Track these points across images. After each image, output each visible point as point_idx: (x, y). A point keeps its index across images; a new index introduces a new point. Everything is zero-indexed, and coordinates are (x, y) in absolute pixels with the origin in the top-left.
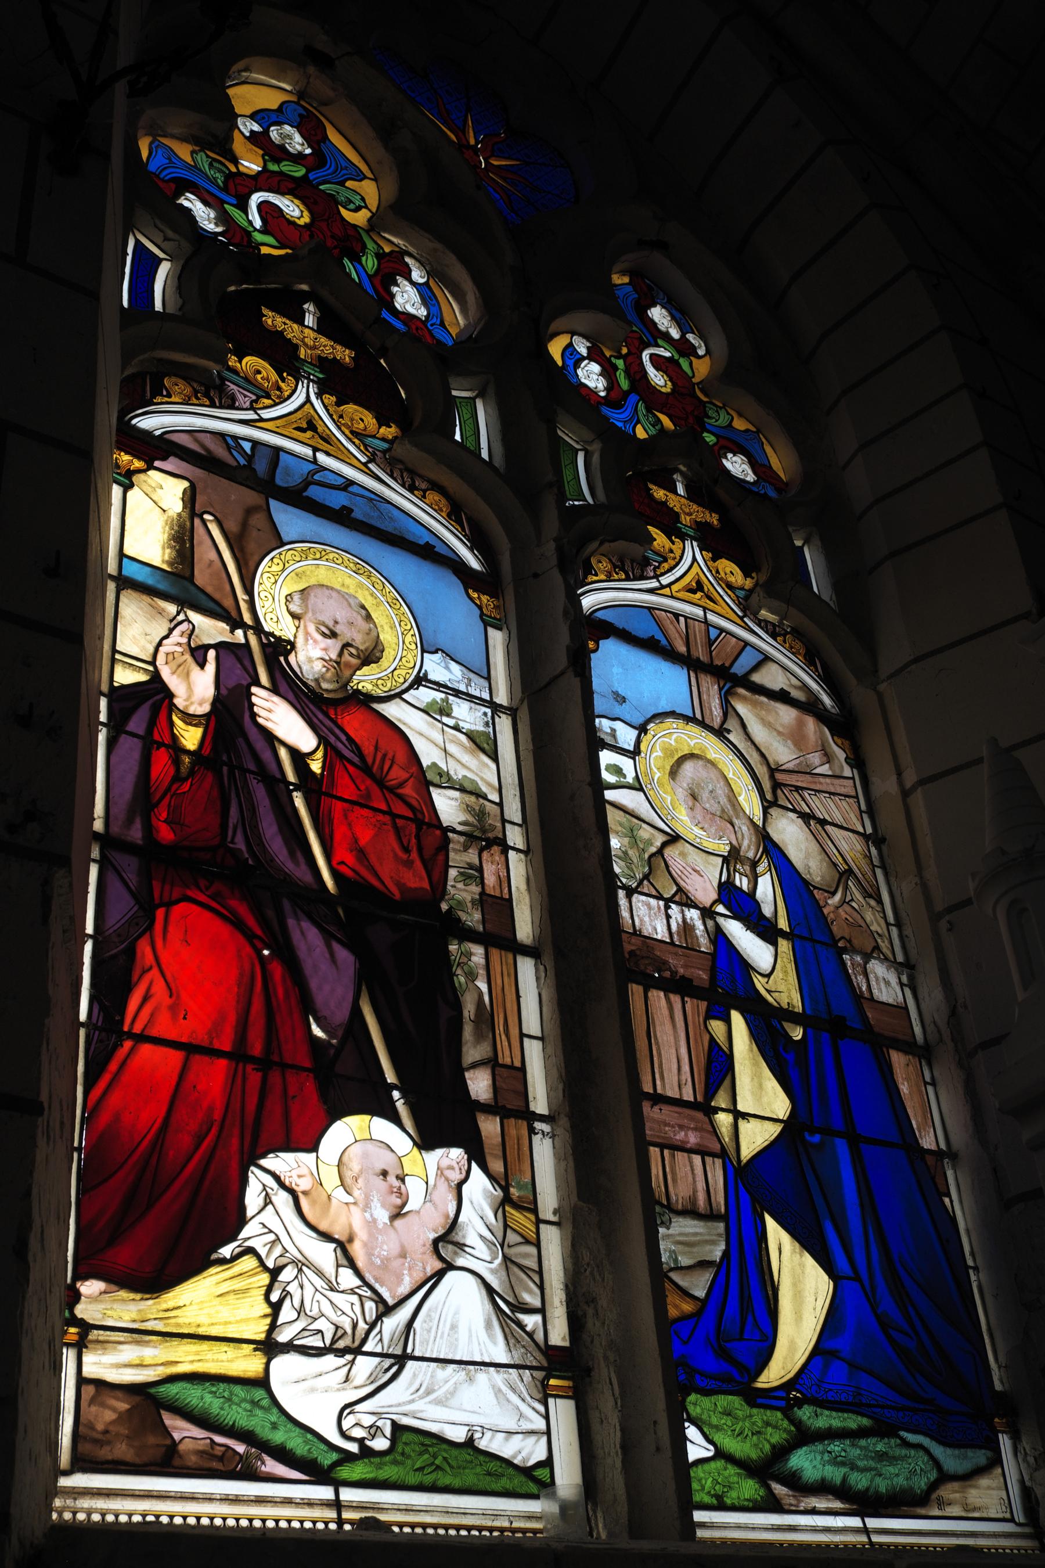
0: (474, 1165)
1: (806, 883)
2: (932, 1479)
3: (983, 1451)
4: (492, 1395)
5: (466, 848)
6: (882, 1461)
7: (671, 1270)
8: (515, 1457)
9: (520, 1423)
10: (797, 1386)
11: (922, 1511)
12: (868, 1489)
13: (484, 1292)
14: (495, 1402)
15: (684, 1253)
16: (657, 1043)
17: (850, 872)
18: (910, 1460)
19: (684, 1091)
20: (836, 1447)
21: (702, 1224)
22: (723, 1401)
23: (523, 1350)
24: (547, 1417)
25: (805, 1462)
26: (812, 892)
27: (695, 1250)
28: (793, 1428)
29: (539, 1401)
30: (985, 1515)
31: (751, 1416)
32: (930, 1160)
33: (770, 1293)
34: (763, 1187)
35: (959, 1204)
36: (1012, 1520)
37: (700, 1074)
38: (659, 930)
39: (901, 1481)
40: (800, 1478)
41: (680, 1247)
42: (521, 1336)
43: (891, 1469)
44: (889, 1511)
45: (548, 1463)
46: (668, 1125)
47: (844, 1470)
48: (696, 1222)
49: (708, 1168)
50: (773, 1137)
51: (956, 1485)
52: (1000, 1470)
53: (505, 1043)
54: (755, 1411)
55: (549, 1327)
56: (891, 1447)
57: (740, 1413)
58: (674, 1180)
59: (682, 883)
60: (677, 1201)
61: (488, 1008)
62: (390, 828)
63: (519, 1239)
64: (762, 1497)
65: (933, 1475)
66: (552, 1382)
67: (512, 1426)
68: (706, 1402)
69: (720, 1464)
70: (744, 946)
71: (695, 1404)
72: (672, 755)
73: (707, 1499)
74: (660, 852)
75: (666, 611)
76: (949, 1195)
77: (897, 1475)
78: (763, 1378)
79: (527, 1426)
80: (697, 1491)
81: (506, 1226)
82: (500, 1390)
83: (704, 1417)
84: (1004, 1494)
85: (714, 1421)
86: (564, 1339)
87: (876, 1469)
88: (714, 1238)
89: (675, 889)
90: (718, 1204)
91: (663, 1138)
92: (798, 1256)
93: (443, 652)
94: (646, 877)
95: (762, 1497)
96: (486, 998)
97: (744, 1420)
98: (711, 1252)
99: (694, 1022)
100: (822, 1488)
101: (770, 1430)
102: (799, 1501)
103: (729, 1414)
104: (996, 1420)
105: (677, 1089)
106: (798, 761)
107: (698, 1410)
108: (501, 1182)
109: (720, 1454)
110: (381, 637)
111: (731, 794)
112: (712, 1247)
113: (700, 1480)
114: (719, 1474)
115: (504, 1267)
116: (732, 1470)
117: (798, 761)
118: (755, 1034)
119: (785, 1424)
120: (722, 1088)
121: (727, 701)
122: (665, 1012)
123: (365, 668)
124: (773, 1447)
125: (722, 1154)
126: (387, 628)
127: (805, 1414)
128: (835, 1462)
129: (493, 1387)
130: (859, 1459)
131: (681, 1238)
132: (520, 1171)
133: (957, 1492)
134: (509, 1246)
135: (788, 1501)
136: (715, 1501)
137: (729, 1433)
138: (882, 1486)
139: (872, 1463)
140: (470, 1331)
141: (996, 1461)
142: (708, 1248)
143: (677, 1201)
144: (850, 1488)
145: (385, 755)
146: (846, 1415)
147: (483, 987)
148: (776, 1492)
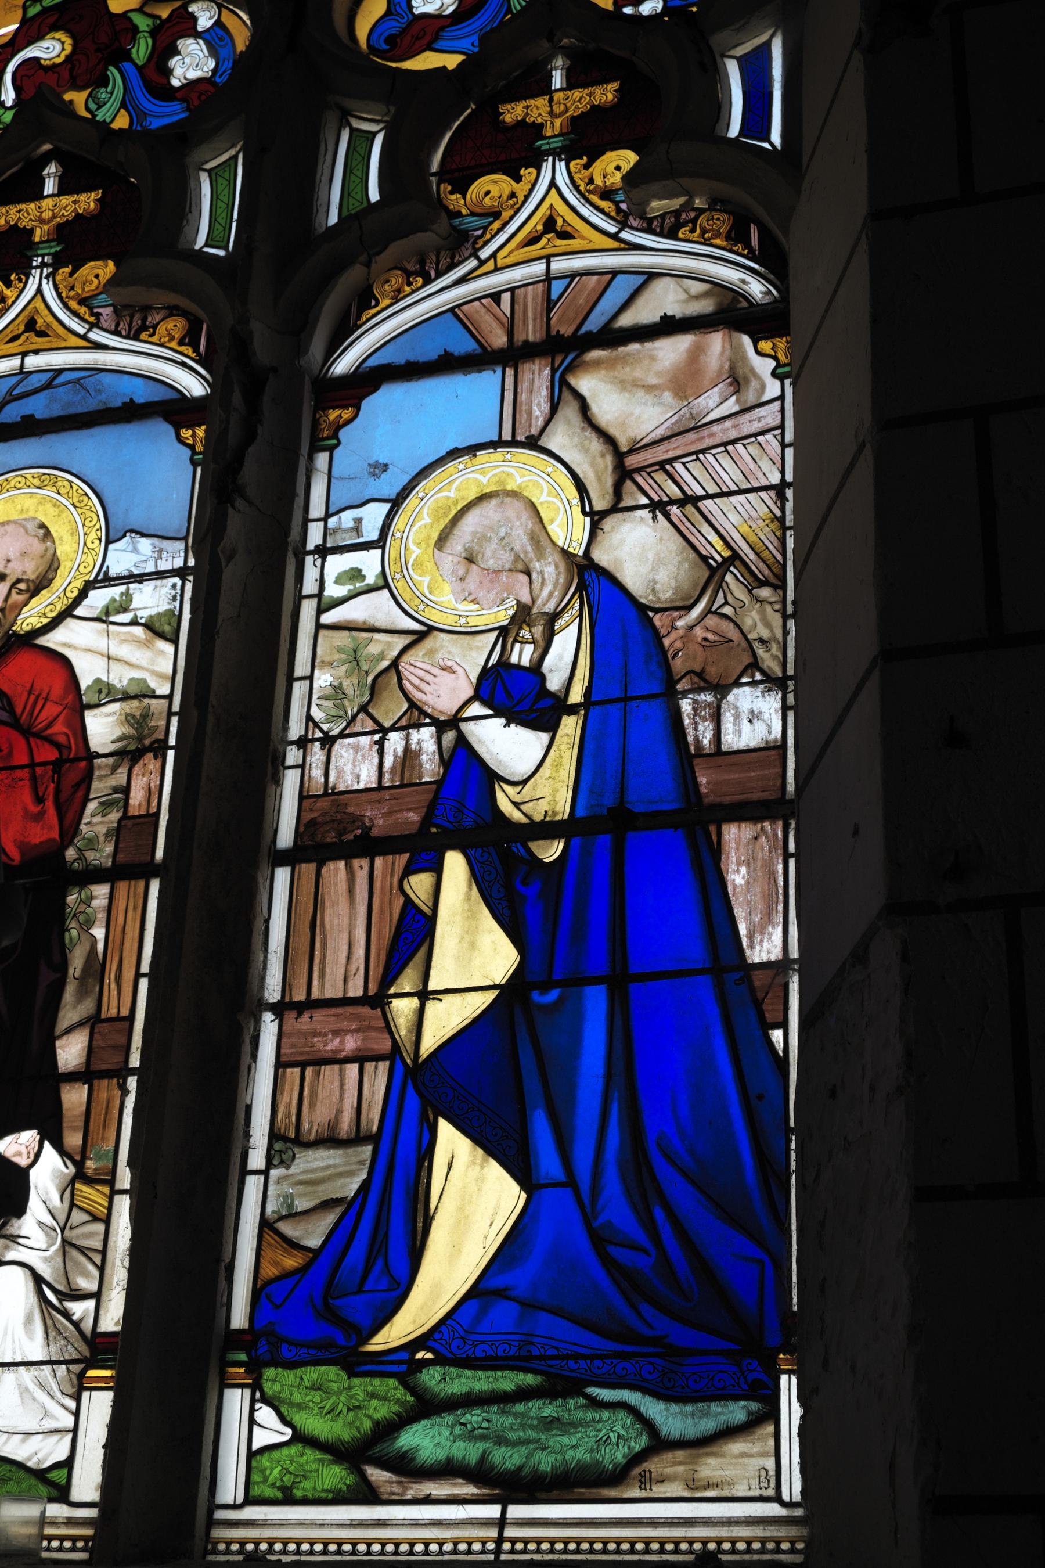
0: (47, 1144)
2: (637, 1448)
3: (742, 1403)
4: (18, 1395)
5: (114, 769)
6: (549, 1430)
7: (281, 1218)
8: (29, 1459)
9: (42, 1423)
11: (613, 1493)
12: (520, 1468)
13: (31, 1284)
14: (18, 1401)
15: (300, 1196)
17: (735, 558)
18: (600, 1425)
20: (474, 1417)
21: (340, 1152)
23: (63, 1342)
24: (77, 1414)
25: (424, 1440)
26: (650, 620)
27: (321, 1188)
29: (70, 1396)
30: (726, 1493)
31: (350, 1388)
33: (420, 1225)
34: (483, 1082)
36: (778, 1499)
37: (379, 955)
39: (581, 1455)
40: (413, 1459)
41: (301, 1188)
42: (65, 1326)
43: (565, 1440)
44: (555, 1494)
45: (68, 1464)
47: (481, 1446)
48: (332, 1152)
49: (366, 1078)
51: (680, 1454)
52: (771, 1429)
53: (114, 993)
54: (356, 1381)
55: (102, 1312)
56: (569, 1411)
57: (335, 1386)
58: (312, 1104)
59: (417, 695)
60: (310, 1130)
61: (101, 956)
62: (27, 783)
63: (86, 1217)
64: (348, 1486)
66: (91, 1373)
67: (32, 1426)
68: (289, 1376)
70: (495, 749)
71: (274, 1381)
73: (269, 1492)
75: (479, 299)
76: (784, 1025)
77: (574, 1447)
78: (379, 1338)
79: (50, 1424)
80: (258, 1483)
81: (72, 1205)
82: (27, 1389)
83: (283, 1395)
84: (770, 1463)
85: (297, 1398)
86: (117, 1324)
87: (537, 1441)
88: (354, 1167)
89: (405, 706)
90: (372, 1120)
91: (308, 1053)
92: (478, 1168)
93: (132, 531)
94: (364, 708)
95: (348, 1486)
96: (100, 946)
97: (339, 1394)
99: (382, 888)
100: (447, 1470)
102: (406, 1489)
103: (319, 1389)
104: (781, 1356)
106: (676, 417)
107: (277, 1387)
108: (76, 1159)
109: (299, 1437)
110: (58, 552)
111: (538, 527)
112: (348, 1180)
114: (292, 1462)
115: (61, 1253)
116: (311, 1455)
117: (676, 417)
119: (401, 1393)
120: (411, 965)
121: (564, 383)
123: (34, 600)
125: (395, 1053)
126: (67, 537)
127: (431, 1378)
128: (471, 1436)
129: (20, 1386)
130: (511, 1429)
132: (103, 1139)
133: (680, 1463)
134: (71, 1228)
135: (389, 1489)
136: (279, 1495)
138: (546, 1462)
139: (531, 1434)
140: (6, 1329)
141: (772, 1414)
143: (310, 1130)
144: (492, 1467)
145: (38, 697)
146: (499, 1373)
147: (99, 932)
148: (373, 1479)
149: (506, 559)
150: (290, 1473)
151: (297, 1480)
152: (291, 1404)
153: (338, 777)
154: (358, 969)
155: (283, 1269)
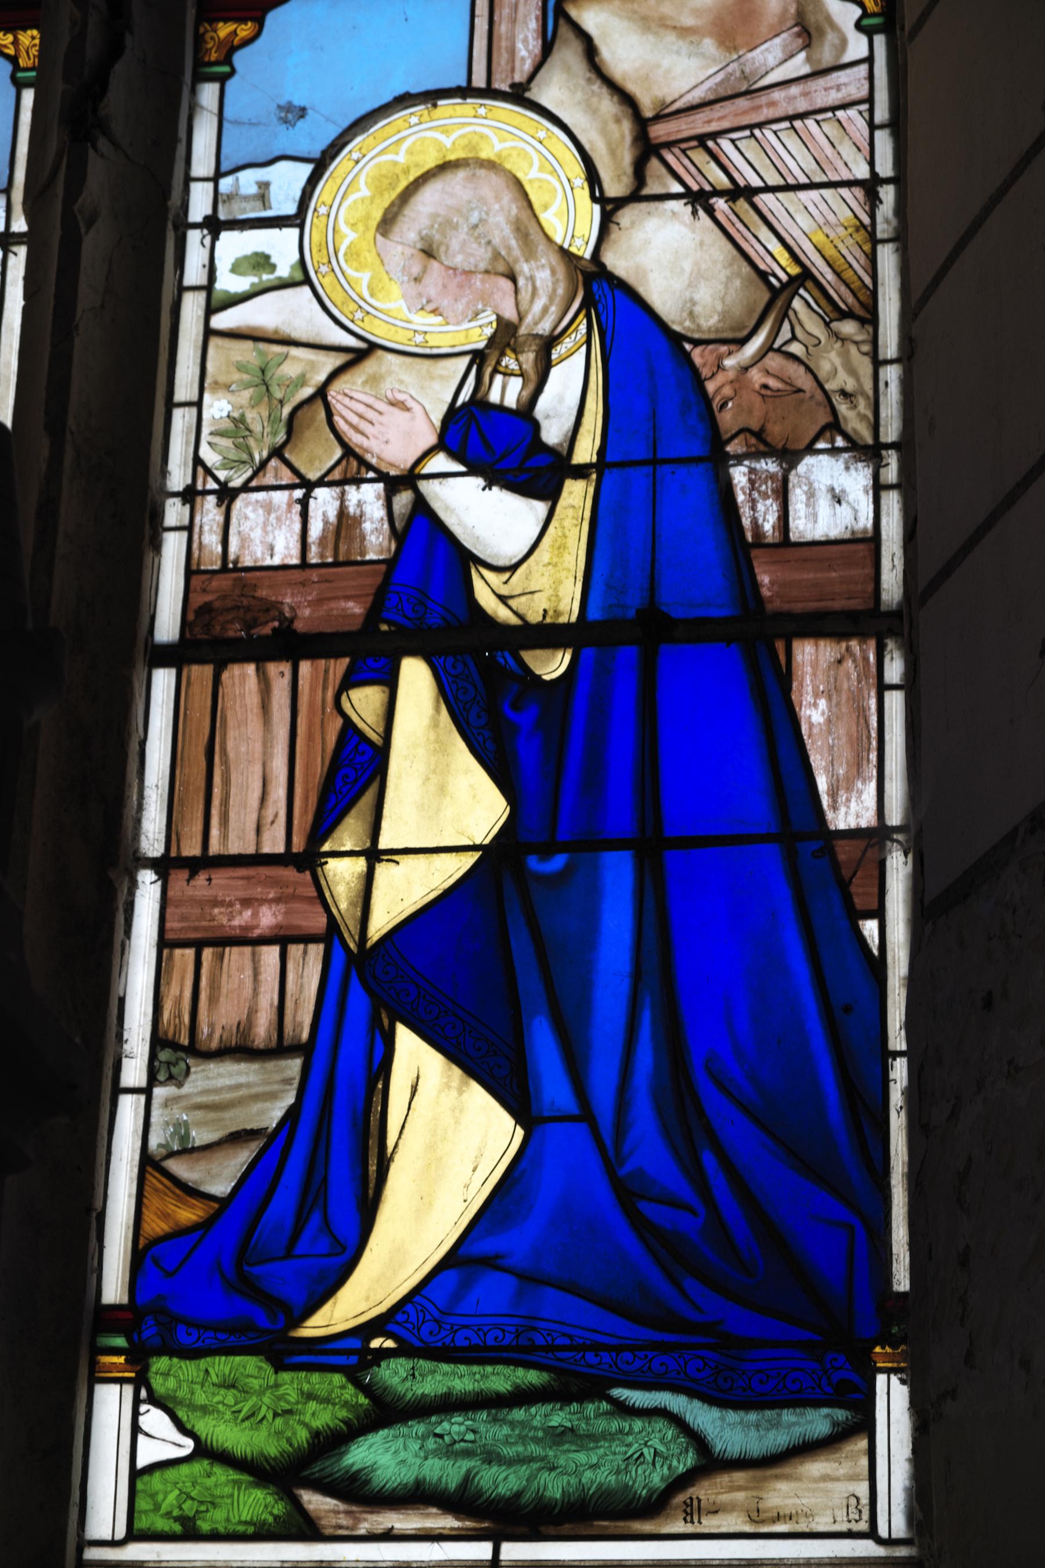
1: (676, 339)
3: (825, 1411)
7: (172, 1154)
10: (391, 1327)
12: (519, 1494)
15: (199, 1124)
16: (225, 762)
17: (805, 276)
19: (266, 836)
20: (455, 1426)
21: (255, 1066)
22: (221, 1366)
25: (383, 1456)
26: (687, 356)
28: (363, 1400)
30: (802, 1527)
32: (844, 852)
33: (373, 1168)
34: (458, 974)
35: (892, 932)
36: (872, 1534)
37: (306, 798)
38: (280, 548)
40: (368, 1482)
41: (199, 1114)
44: (567, 1529)
46: (215, 903)
48: (243, 1066)
50: (451, 881)
51: (740, 1477)
52: (863, 1444)
54: (286, 1376)
56: (588, 1419)
57: (255, 1383)
58: (213, 1000)
60: (210, 1036)
65: (690, 1460)
68: (189, 1369)
69: (200, 1467)
70: (470, 520)
71: (166, 1375)
72: (392, 186)
73: (162, 1524)
74: (321, 393)
76: (879, 913)
77: (594, 1467)
80: (146, 1512)
83: (180, 1394)
84: (862, 1489)
85: (200, 1398)
89: (338, 453)
92: (454, 1093)
94: (277, 452)
97: (261, 1393)
98: (262, 1113)
101: (312, 1405)
102: (357, 1521)
103: (233, 1386)
104: (878, 1349)
105: (252, 835)
107: (171, 1383)
109: (203, 1451)
111: (525, 215)
112: (268, 1104)
113: (153, 1496)
114: (194, 1484)
116: (222, 1474)
118: (451, 694)
119: (350, 1393)
120: (354, 812)
122: (253, 699)
124: (316, 1434)
125: (331, 934)
128: (450, 1451)
131: (199, 1100)
133: (740, 1488)
135: (334, 1522)
136: (177, 1528)
137: (228, 1416)
139: (534, 1449)
141: (863, 1424)
142: (256, 1107)
143: (210, 1036)
144: (480, 1493)
149: (481, 256)
150: (193, 1499)
151: (203, 1508)
152: (192, 1407)
153: (242, 547)
154: (276, 816)
155: (177, 1223)
